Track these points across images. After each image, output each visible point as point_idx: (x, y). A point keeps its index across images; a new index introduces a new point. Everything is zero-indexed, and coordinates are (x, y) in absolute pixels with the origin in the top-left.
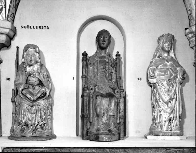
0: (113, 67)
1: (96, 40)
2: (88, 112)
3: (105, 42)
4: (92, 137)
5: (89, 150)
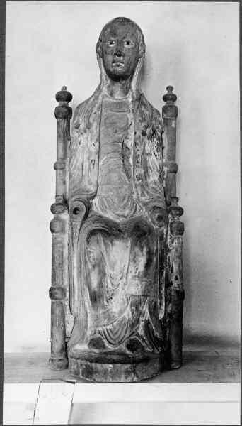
0: (151, 137)
1: (97, 52)
2: (66, 282)
3: (122, 58)
4: (76, 366)
5: (190, 367)
